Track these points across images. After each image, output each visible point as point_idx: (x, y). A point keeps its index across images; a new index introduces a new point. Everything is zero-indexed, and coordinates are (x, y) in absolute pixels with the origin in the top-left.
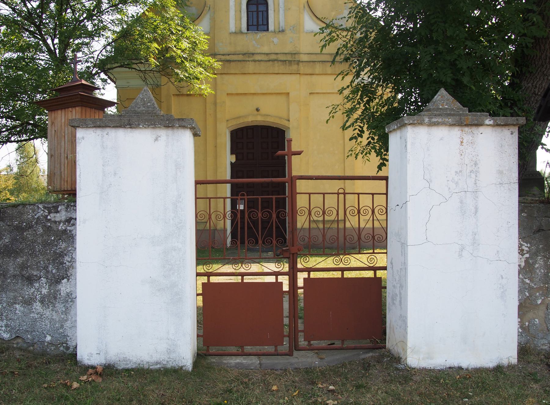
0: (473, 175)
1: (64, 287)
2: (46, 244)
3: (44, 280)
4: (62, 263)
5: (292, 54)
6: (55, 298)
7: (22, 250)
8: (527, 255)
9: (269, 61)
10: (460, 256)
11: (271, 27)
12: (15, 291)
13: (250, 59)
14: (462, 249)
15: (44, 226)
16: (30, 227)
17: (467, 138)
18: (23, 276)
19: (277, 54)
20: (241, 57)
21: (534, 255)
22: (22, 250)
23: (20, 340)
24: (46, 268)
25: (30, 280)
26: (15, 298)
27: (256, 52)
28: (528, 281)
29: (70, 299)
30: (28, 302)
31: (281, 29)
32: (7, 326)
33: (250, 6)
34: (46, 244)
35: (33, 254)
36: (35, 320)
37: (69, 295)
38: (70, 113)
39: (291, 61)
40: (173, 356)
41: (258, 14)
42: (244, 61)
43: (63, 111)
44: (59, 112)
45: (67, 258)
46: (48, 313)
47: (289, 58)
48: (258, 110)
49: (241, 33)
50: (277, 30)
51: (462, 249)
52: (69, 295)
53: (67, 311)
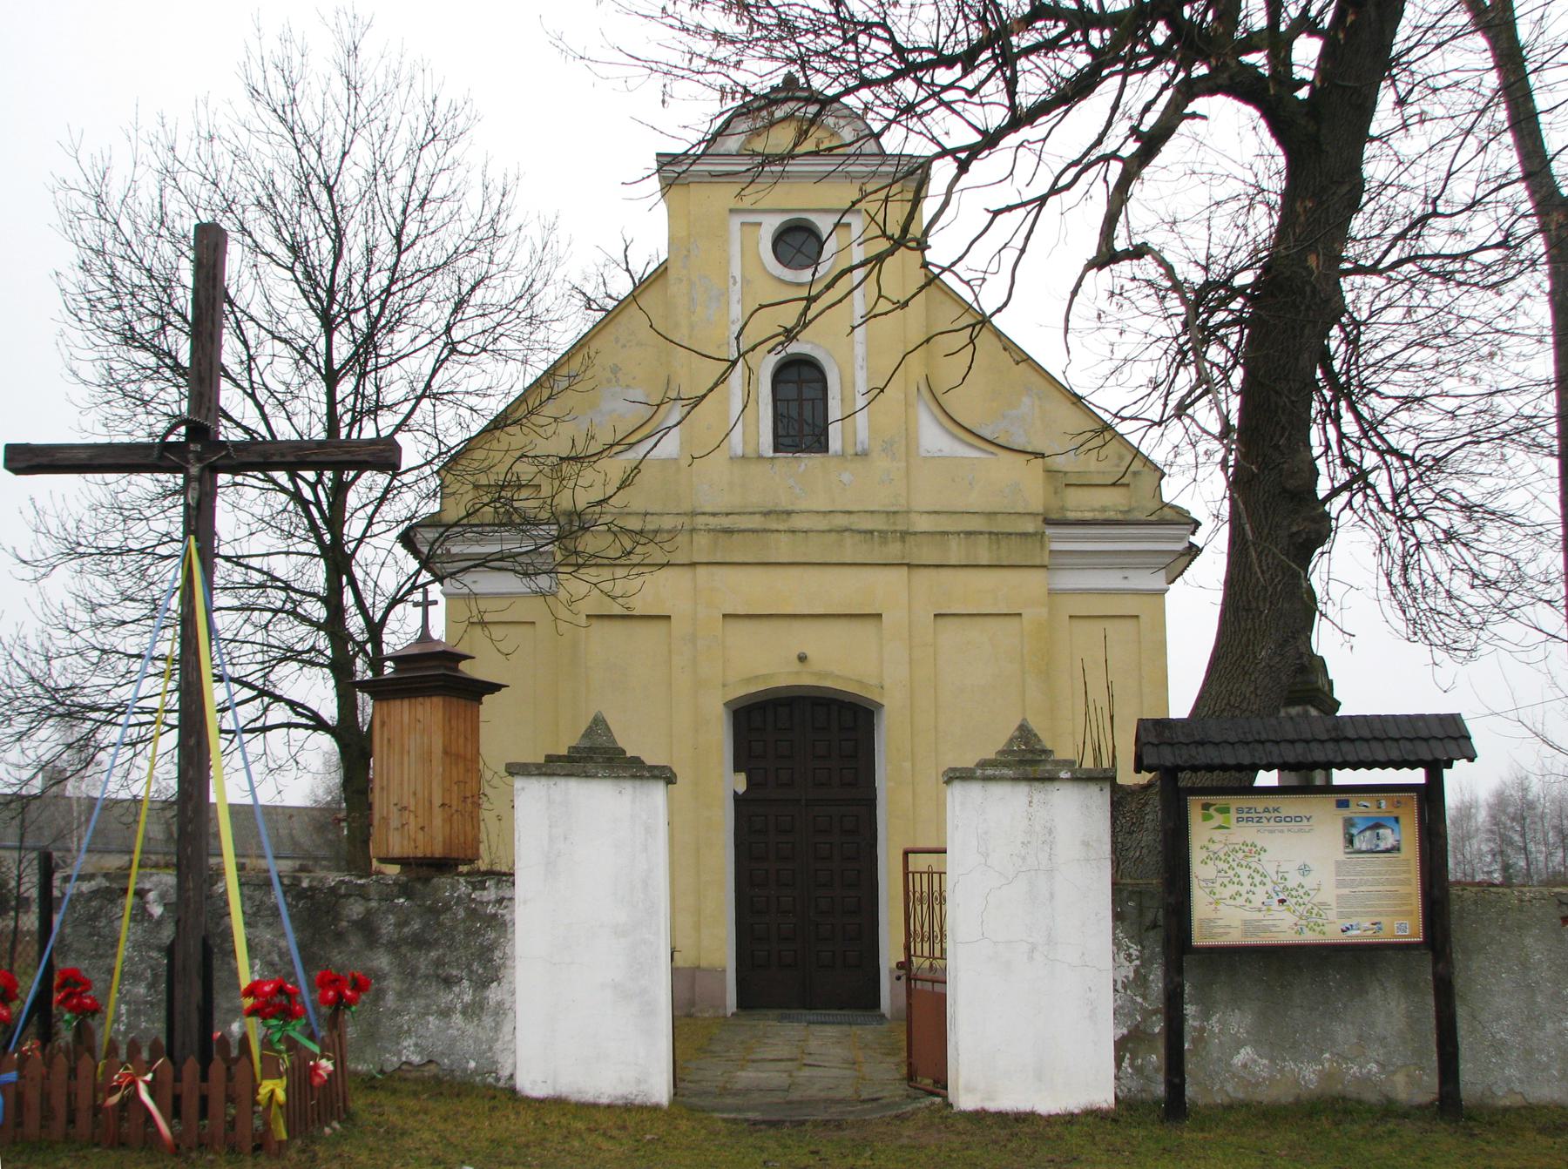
0: (1047, 848)
1: (494, 994)
2: (469, 933)
3: (466, 983)
4: (491, 960)
5: (887, 513)
6: (482, 1009)
7: (437, 941)
8: (1137, 962)
9: (830, 531)
10: (1031, 959)
11: (835, 443)
12: (428, 996)
13: (781, 527)
14: (1033, 949)
15: (467, 909)
16: (446, 908)
17: (1037, 797)
18: (438, 976)
19: (850, 513)
20: (756, 522)
21: (1146, 962)
22: (437, 941)
23: (432, 1067)
24: (469, 966)
25: (448, 982)
26: (428, 1007)
27: (796, 508)
28: (1139, 1000)
29: (501, 1011)
30: (445, 1013)
31: (859, 448)
32: (416, 1045)
33: (781, 387)
34: (469, 933)
35: (451, 947)
36: (454, 1039)
37: (500, 1004)
38: (420, 708)
39: (886, 532)
40: (643, 1087)
41: (801, 407)
42: (765, 531)
43: (406, 702)
44: (398, 703)
45: (498, 954)
46: (471, 1029)
47: (878, 524)
48: (802, 658)
49: (760, 457)
50: (851, 451)
51: (1033, 949)
52: (500, 1004)
53: (497, 1028)
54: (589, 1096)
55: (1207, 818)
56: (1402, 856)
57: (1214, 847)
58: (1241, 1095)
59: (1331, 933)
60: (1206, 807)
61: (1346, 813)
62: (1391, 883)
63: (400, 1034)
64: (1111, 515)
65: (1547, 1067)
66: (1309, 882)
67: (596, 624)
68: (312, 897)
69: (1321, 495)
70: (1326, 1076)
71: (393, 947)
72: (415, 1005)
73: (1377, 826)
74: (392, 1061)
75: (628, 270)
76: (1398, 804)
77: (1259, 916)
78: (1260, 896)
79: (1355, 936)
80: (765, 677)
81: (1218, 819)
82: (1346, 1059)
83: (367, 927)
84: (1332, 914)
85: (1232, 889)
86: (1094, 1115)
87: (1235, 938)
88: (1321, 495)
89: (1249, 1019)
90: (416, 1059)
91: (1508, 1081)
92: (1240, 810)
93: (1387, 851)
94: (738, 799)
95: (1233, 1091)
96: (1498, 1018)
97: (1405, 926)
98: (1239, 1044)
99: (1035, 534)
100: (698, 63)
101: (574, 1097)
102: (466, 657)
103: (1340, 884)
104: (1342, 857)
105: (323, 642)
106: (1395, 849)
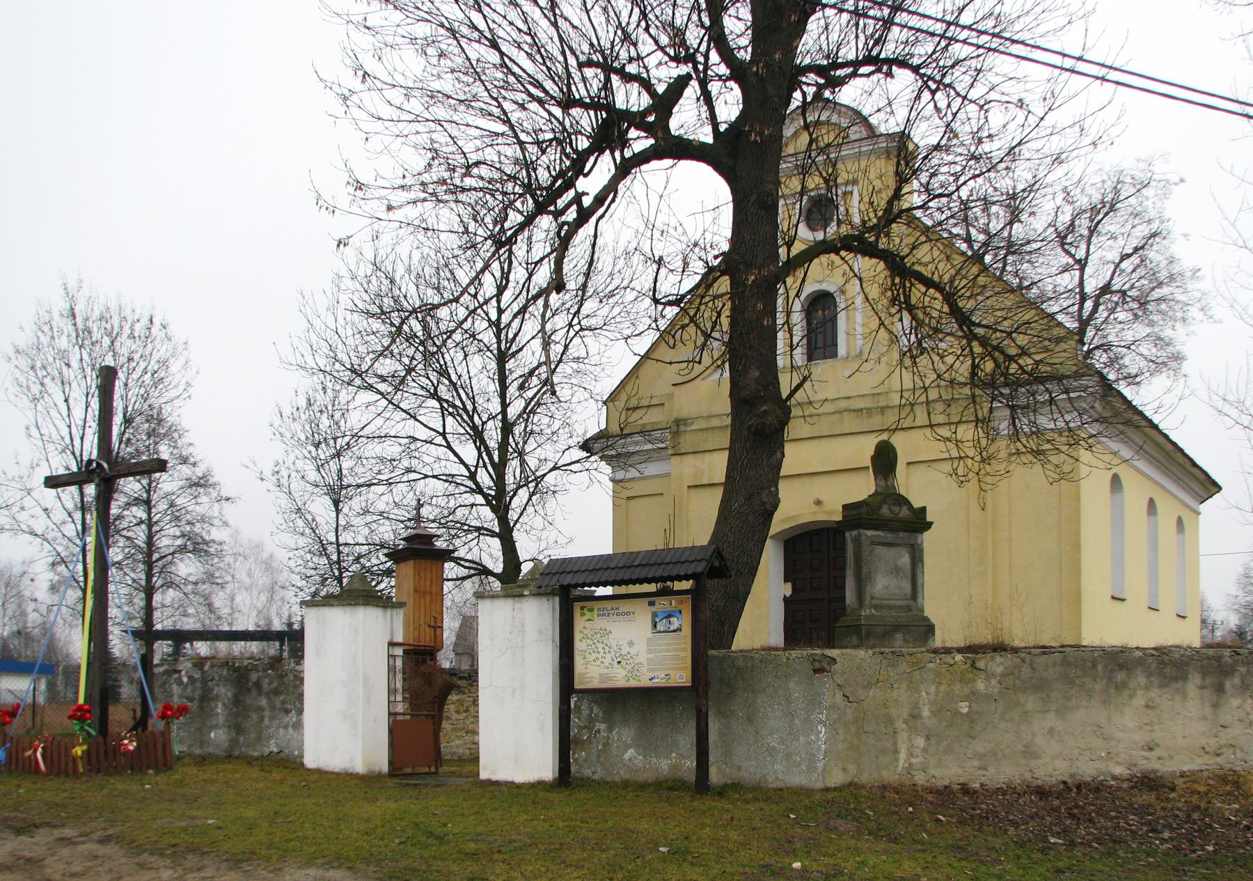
11: (842, 350)
14: (514, 691)
17: (517, 606)
25: (287, 712)
30: (286, 727)
35: (288, 694)
48: (818, 503)
51: (514, 691)
54: (331, 768)
55: (582, 615)
56: (682, 634)
57: (586, 632)
58: (628, 777)
59: (644, 681)
60: (582, 608)
61: (653, 609)
62: (675, 650)
63: (270, 737)
65: (799, 765)
66: (633, 651)
67: (693, 491)
69: (784, 396)
70: (674, 767)
71: (267, 694)
72: (275, 723)
73: (669, 616)
74: (267, 751)
76: (681, 602)
77: (607, 671)
78: (607, 661)
79: (657, 682)
80: (798, 516)
81: (588, 615)
82: (684, 757)
83: (258, 685)
84: (644, 670)
85: (594, 656)
86: (539, 785)
87: (595, 684)
88: (784, 396)
89: (633, 732)
90: (275, 750)
91: (776, 772)
92: (599, 610)
93: (674, 631)
94: (785, 599)
95: (624, 774)
96: (771, 734)
97: (682, 677)
98: (628, 747)
100: (46, 328)
101: (326, 769)
103: (649, 651)
104: (650, 635)
106: (679, 630)
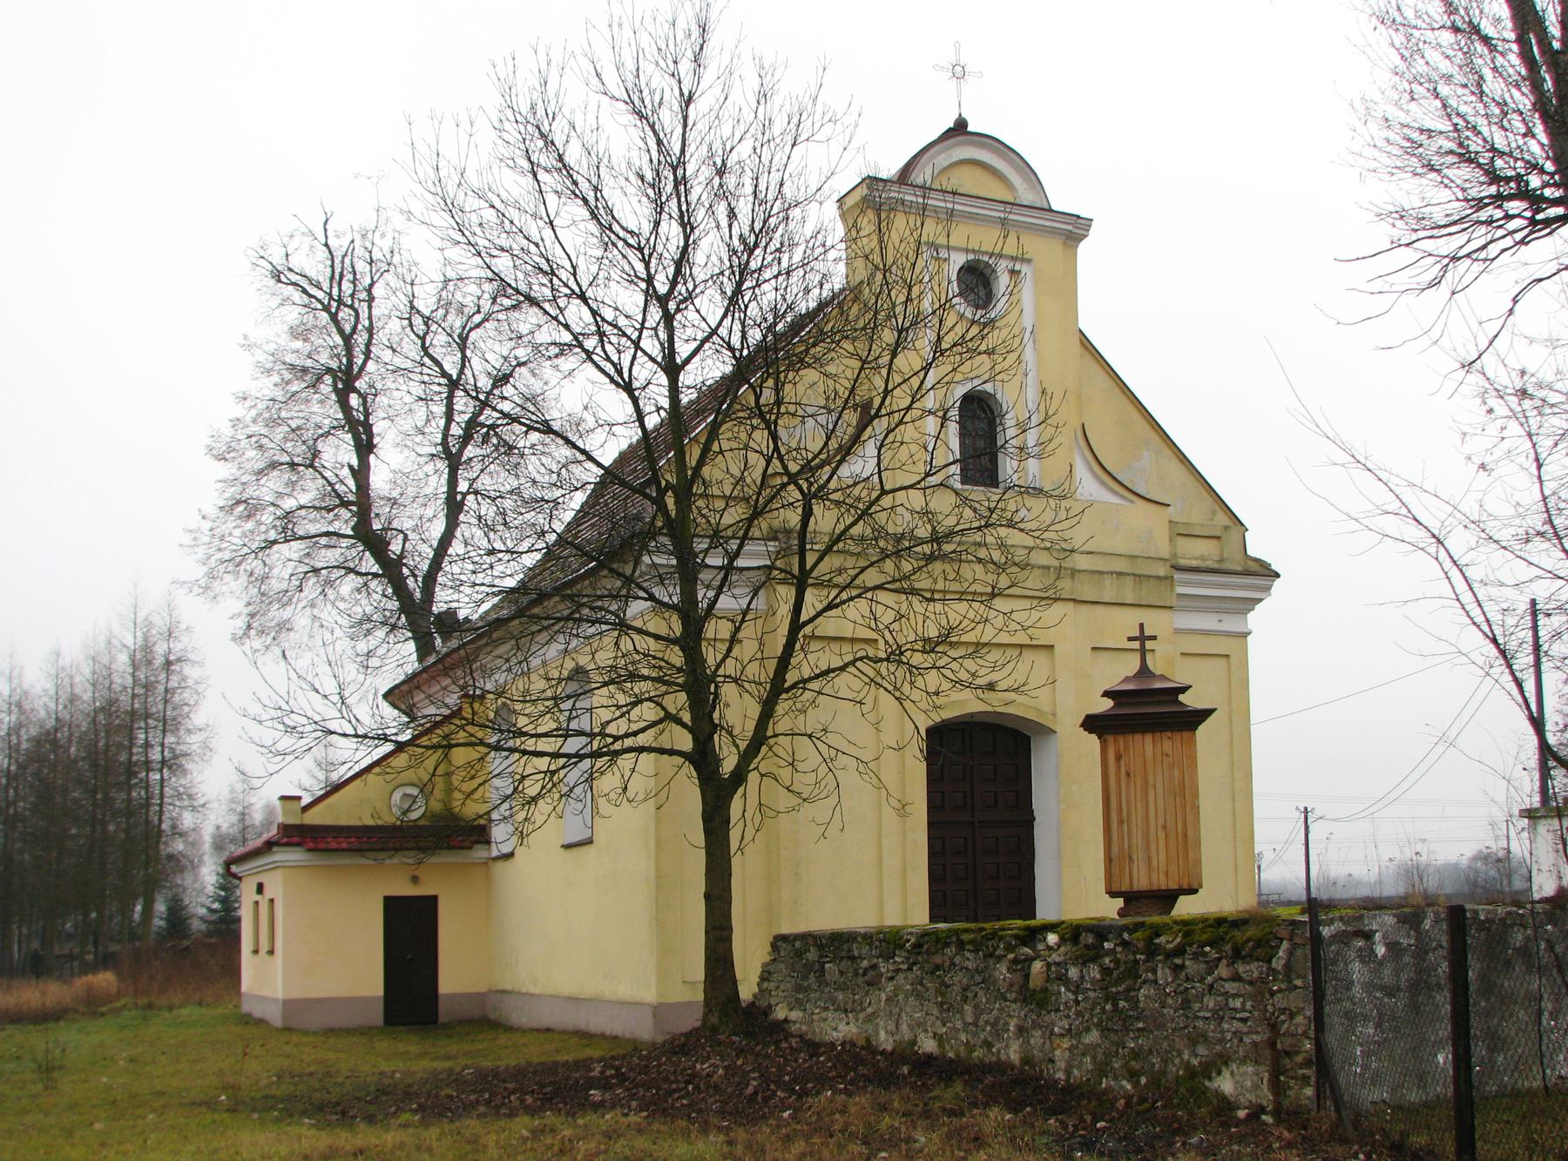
44: (1138, 737)
64: (1210, 564)
68: (1489, 930)
75: (326, 245)
99: (1165, 578)
102: (1184, 690)
105: (676, 657)
